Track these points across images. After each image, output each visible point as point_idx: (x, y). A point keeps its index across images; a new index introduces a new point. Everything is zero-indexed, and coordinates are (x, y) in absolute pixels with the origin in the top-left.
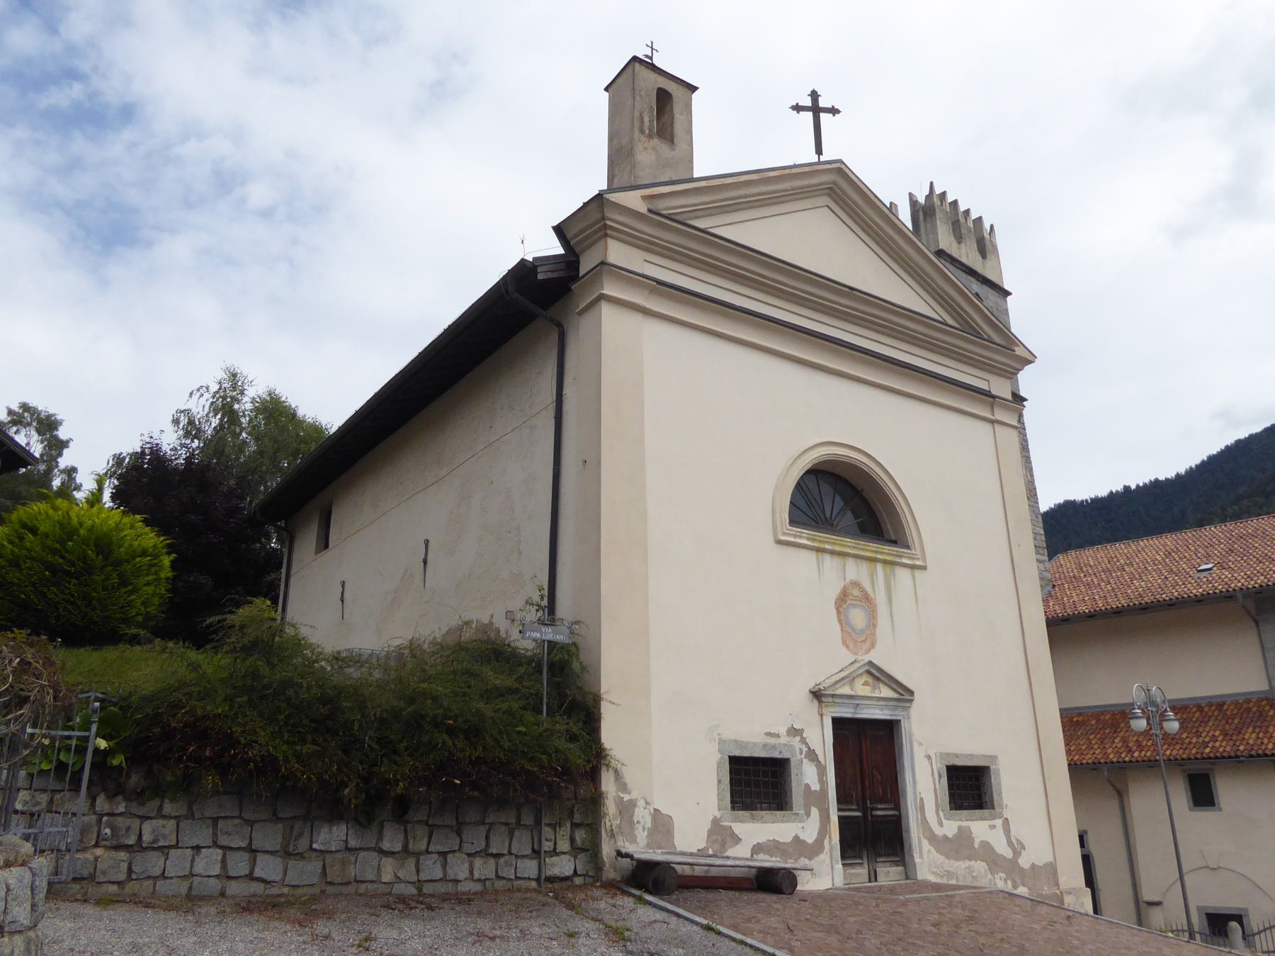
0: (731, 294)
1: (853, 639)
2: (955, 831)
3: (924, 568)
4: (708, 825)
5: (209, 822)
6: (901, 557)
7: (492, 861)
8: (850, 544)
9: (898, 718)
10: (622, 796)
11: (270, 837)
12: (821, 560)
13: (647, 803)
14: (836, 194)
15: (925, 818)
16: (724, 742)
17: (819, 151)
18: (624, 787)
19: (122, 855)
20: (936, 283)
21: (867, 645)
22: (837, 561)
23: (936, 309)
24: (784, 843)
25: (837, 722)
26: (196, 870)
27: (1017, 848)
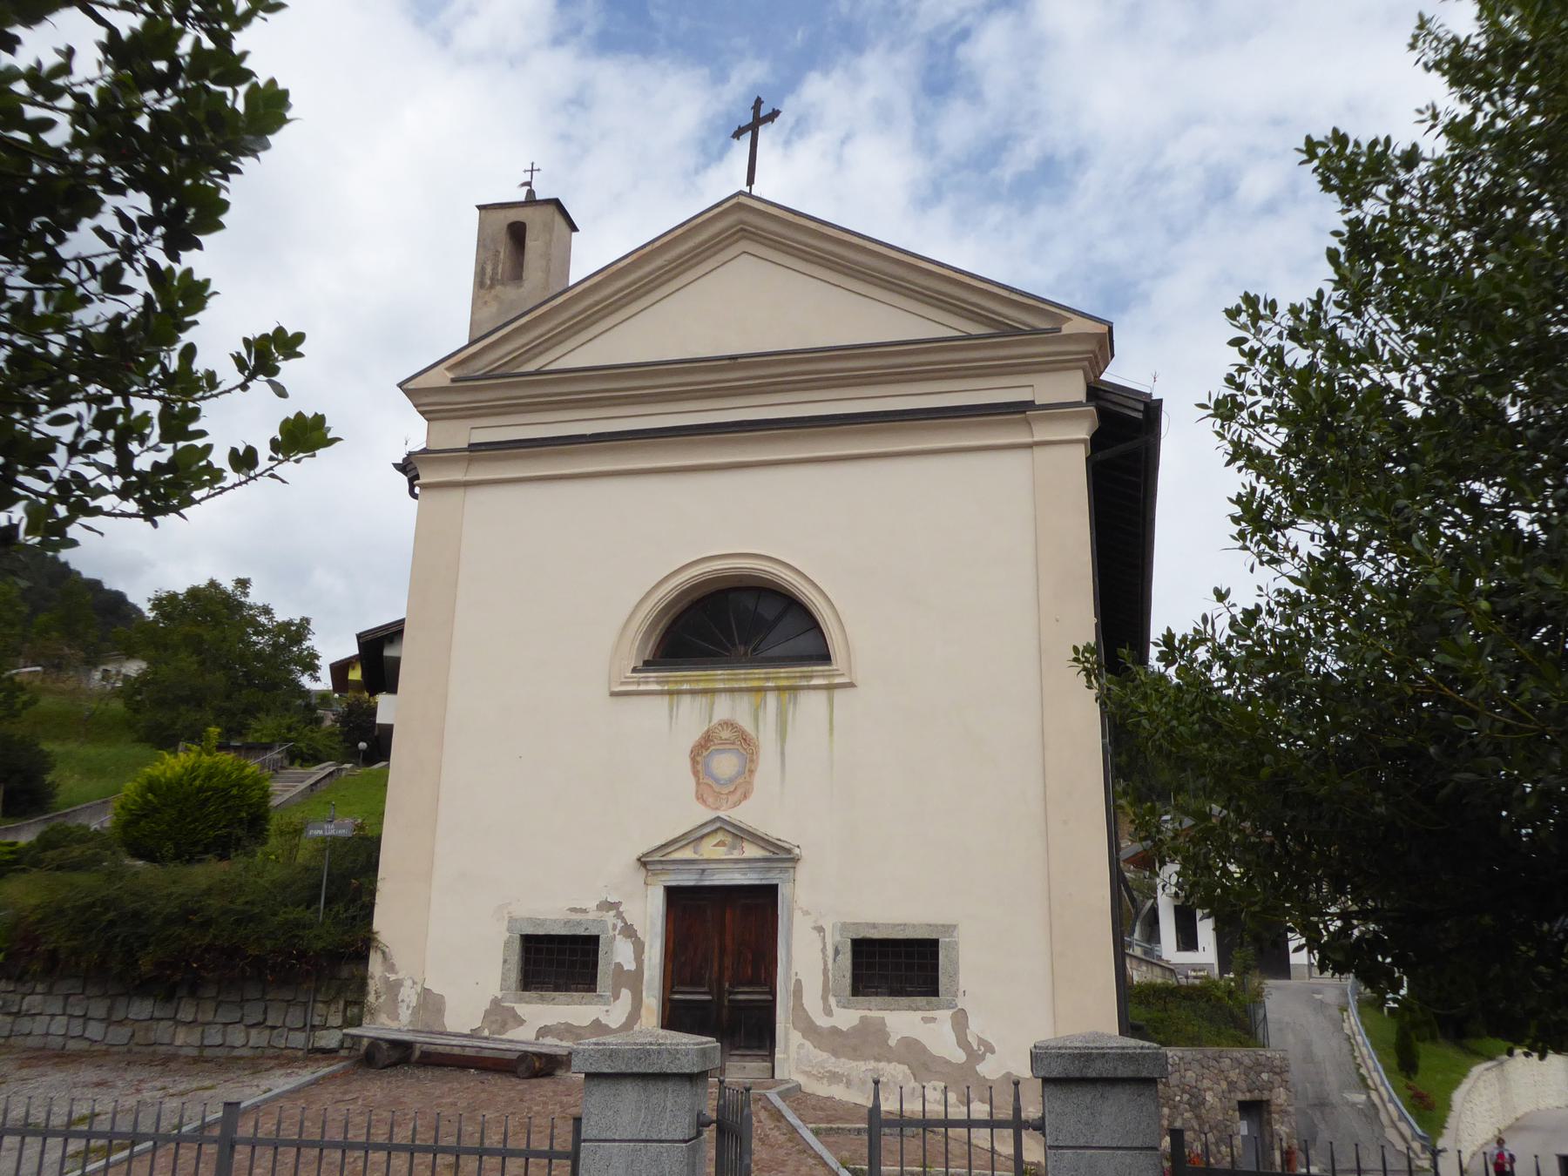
3: (851, 685)
4: (486, 1005)
5: (61, 998)
6: (811, 677)
7: (267, 1032)
9: (774, 882)
11: (98, 1009)
17: (750, 181)
18: (391, 968)
19: (9, 1019)
20: (916, 285)
22: (702, 701)
25: (672, 893)
26: (51, 1031)
27: (976, 1053)
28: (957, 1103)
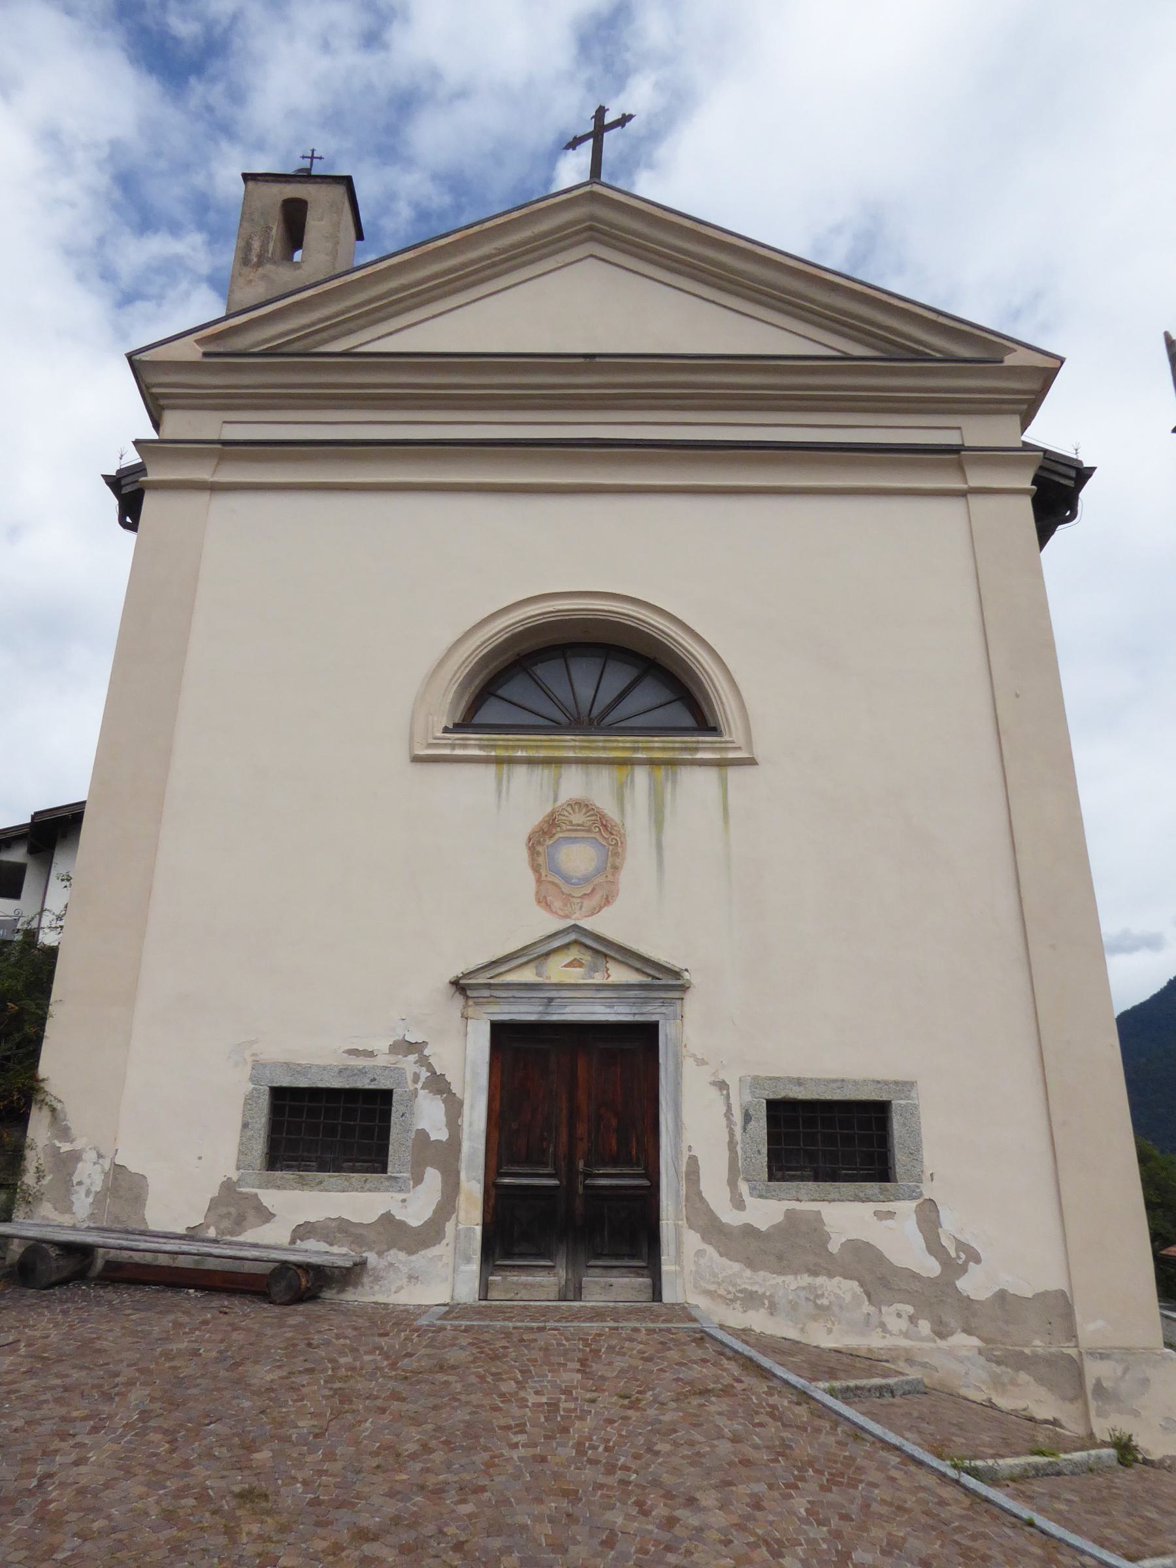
0: (353, 427)
1: (563, 893)
2: (779, 1218)
3: (751, 762)
6: (696, 750)
8: (573, 744)
9: (654, 1018)
10: (58, 1144)
12: (505, 776)
13: (100, 1156)
14: (598, 230)
15: (699, 1193)
16: (264, 1065)
18: (64, 1133)
21: (596, 899)
22: (543, 774)
23: (384, 332)
24: (361, 1225)
25: (498, 1029)
28: (933, 1335)
